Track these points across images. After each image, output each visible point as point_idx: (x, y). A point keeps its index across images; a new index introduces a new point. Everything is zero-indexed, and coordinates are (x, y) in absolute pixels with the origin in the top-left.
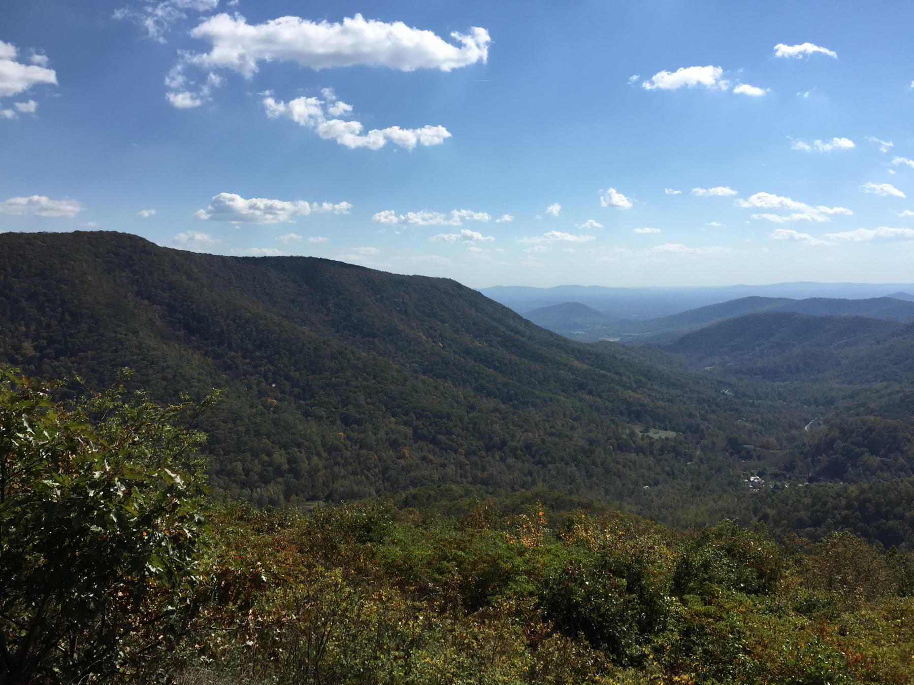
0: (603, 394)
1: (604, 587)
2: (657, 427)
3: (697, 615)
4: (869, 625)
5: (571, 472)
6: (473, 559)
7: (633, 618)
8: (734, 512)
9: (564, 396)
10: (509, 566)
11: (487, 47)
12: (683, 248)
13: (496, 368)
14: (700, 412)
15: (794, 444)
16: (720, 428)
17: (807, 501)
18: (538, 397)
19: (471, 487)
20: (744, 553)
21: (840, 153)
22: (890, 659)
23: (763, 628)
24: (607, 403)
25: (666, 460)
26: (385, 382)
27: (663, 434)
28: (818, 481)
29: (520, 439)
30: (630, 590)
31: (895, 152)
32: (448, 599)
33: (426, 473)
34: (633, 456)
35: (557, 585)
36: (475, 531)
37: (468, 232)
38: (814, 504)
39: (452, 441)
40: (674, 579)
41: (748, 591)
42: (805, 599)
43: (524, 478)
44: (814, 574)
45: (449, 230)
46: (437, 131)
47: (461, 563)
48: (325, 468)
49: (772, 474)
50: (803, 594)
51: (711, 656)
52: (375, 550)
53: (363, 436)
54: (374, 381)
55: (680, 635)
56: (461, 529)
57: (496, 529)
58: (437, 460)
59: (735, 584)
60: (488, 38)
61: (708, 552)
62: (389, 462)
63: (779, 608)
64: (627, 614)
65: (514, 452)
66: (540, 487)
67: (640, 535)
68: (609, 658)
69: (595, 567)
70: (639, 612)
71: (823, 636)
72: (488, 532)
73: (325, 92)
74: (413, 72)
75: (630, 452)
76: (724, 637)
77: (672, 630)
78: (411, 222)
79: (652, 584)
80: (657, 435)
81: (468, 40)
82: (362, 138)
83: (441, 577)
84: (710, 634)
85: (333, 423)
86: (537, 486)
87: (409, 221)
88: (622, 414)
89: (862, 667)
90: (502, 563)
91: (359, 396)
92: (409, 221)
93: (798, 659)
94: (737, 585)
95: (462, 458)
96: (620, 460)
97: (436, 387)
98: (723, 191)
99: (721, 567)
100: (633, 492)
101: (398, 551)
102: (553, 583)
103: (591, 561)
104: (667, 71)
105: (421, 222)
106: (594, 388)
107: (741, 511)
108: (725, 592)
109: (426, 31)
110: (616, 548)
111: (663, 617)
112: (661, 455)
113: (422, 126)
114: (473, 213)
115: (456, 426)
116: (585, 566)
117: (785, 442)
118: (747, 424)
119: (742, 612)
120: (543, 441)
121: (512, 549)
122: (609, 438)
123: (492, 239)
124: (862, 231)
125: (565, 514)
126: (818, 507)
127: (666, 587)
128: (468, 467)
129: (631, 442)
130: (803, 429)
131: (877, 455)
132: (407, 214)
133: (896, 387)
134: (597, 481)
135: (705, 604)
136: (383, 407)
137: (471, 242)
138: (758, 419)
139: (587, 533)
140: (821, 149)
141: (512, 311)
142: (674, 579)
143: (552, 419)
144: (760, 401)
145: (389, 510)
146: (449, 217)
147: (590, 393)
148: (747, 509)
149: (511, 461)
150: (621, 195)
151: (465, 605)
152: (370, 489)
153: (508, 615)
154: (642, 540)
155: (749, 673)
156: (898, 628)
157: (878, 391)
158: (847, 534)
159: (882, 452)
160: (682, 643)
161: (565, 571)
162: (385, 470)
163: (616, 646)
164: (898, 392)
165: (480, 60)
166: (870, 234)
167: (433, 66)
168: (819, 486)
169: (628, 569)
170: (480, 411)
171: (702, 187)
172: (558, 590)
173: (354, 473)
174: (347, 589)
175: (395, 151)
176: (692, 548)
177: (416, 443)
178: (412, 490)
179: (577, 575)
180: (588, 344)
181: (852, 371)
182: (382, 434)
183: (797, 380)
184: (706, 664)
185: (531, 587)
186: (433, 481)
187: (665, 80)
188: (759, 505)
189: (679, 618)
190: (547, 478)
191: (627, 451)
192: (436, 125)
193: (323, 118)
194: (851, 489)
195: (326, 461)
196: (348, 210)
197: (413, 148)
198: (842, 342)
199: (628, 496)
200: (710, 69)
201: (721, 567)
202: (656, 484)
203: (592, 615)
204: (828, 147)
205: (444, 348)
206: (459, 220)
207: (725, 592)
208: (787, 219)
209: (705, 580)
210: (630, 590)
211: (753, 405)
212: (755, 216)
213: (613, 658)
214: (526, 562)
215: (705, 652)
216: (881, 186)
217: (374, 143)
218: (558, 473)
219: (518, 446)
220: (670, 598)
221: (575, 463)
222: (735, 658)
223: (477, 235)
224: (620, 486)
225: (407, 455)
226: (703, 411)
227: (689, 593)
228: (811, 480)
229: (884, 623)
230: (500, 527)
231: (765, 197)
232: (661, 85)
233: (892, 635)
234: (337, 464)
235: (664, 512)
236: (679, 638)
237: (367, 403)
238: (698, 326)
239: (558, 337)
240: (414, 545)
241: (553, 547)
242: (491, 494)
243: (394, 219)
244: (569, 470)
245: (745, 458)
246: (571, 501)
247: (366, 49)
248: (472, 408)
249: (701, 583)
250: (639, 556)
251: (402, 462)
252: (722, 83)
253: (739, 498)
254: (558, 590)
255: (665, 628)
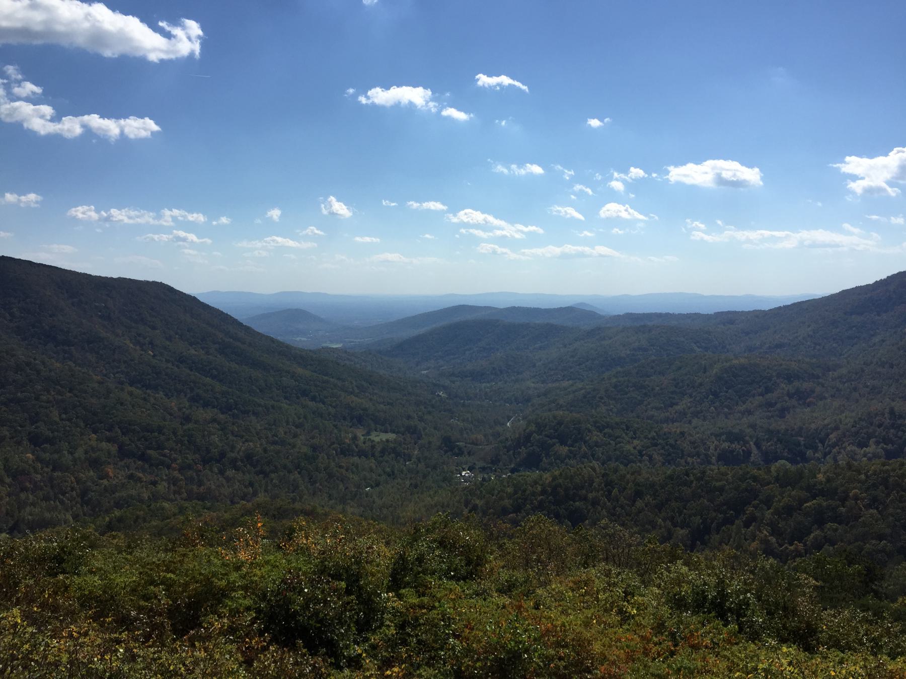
0: (326, 400)
1: (323, 592)
2: (378, 429)
3: (412, 608)
4: (559, 598)
5: (294, 480)
6: (185, 580)
7: (351, 619)
8: (448, 506)
9: (286, 403)
10: (223, 583)
11: (199, 41)
12: (400, 258)
13: (213, 377)
14: (417, 414)
15: (498, 439)
16: (435, 428)
17: (510, 490)
18: (259, 405)
19: (186, 504)
20: (454, 544)
21: (531, 176)
22: (576, 625)
23: (470, 611)
24: (331, 409)
25: (387, 462)
26: (84, 395)
27: (384, 437)
28: (518, 471)
29: (240, 450)
30: (348, 592)
31: (575, 180)
32: (154, 627)
33: (134, 492)
34: (356, 459)
35: (275, 596)
36: (188, 550)
37: (182, 234)
38: (516, 492)
39: (164, 455)
40: (391, 576)
41: (457, 578)
42: (506, 580)
43: (245, 490)
44: (514, 556)
45: (159, 229)
46: (144, 123)
47: (171, 586)
48: (9, 495)
49: (480, 468)
50: (504, 575)
51: (424, 646)
52: (68, 582)
53: (56, 456)
54: (70, 394)
55: (396, 630)
56: (172, 550)
57: (212, 546)
58: (146, 478)
59: (446, 574)
60: (200, 32)
61: (423, 545)
62: (89, 484)
63: (485, 591)
64: (345, 616)
65: (233, 464)
66: (262, 498)
67: (360, 536)
68: (327, 662)
69: (314, 573)
70: (357, 613)
71: (521, 612)
72: (203, 550)
73: (8, 69)
74: (115, 58)
75: (353, 456)
76: (436, 625)
77: (388, 626)
78: (114, 219)
79: (370, 583)
80: (378, 437)
81: (177, 31)
82: (54, 124)
83: (147, 604)
84: (424, 624)
85: (19, 443)
86: (258, 497)
87: (111, 218)
88: (345, 418)
89: (553, 636)
90: (216, 581)
91: (51, 412)
92: (111, 218)
93: (500, 637)
94: (448, 574)
95: (176, 474)
96: (342, 464)
97: (145, 399)
98: (435, 206)
99: (433, 559)
100: (355, 495)
101: (97, 580)
102: (271, 595)
103: (311, 568)
104: (381, 88)
105: (126, 220)
106: (317, 394)
107: (454, 504)
108: (437, 582)
109: (130, 17)
110: (337, 552)
111: (380, 614)
112: (382, 457)
113: (126, 117)
114: (187, 214)
115: (168, 439)
116: (304, 574)
117: (491, 438)
118: (459, 423)
119: (453, 600)
120: (265, 450)
121: (227, 565)
122: (334, 443)
123: (209, 241)
124: (551, 248)
125: (287, 523)
126: (519, 495)
127: (383, 584)
128: (183, 483)
129: (354, 447)
130: (506, 425)
131: (566, 445)
132: (110, 210)
133: (579, 385)
134: (320, 487)
135: (419, 597)
136: (82, 424)
137: (185, 243)
138: (468, 418)
139: (307, 539)
140: (516, 173)
141: (231, 317)
142: (391, 576)
143: (273, 427)
144: (469, 401)
145: (88, 537)
146: (159, 217)
147: (313, 399)
148: (459, 502)
149: (230, 473)
150: (342, 204)
151: (175, 631)
152: (65, 516)
153: (219, 634)
154: (362, 542)
155: (457, 656)
156: (582, 597)
157: (565, 389)
158: (541, 516)
159: (569, 442)
160: (398, 637)
161: (284, 581)
162: (84, 493)
163: (334, 649)
164: (581, 389)
165: (192, 54)
166: (558, 250)
167: (139, 54)
168: (519, 476)
169: (347, 571)
170: (196, 422)
171: (416, 201)
172: (277, 601)
173: (46, 498)
174: (30, 629)
175: (94, 141)
176: (409, 543)
177: (121, 460)
178: (117, 513)
179: (296, 584)
180: (310, 351)
181: (545, 372)
182: (80, 453)
183: (500, 381)
184: (420, 653)
185: (248, 602)
186: (141, 501)
187: (380, 96)
188: (470, 497)
189: (395, 612)
190: (269, 488)
191: (349, 455)
192: (142, 118)
193: (6, 99)
194: (545, 477)
195: (9, 487)
196: (37, 202)
197: (116, 140)
198: (537, 346)
199: (351, 499)
200: (420, 90)
201: (433, 559)
202: (378, 485)
203: (310, 622)
204: (523, 172)
205: (154, 356)
206: (170, 219)
207: (437, 582)
208: (491, 234)
209: (419, 573)
210: (348, 592)
211: (463, 405)
212: (463, 231)
213: (331, 662)
214: (243, 577)
215: (419, 642)
216: (565, 209)
217: (69, 130)
218: (280, 482)
219: (239, 457)
220: (387, 594)
221: (298, 470)
222: (446, 643)
223: (192, 237)
224: (343, 490)
225: (111, 474)
226: (420, 413)
227: (404, 588)
228: (513, 471)
229: (570, 594)
230: (218, 543)
231: (471, 213)
232: (377, 101)
233: (577, 604)
234: (24, 489)
235: (385, 511)
236: (395, 632)
237: (62, 420)
238: (414, 332)
239: (280, 344)
240: (116, 573)
241: (272, 557)
242: (208, 509)
243: (94, 215)
244: (292, 477)
245: (457, 455)
246: (294, 509)
247: (60, 28)
248: (187, 419)
249: (415, 576)
250: (358, 557)
251: (105, 482)
252: (431, 104)
253: (452, 493)
254: (277, 601)
255: (382, 624)
